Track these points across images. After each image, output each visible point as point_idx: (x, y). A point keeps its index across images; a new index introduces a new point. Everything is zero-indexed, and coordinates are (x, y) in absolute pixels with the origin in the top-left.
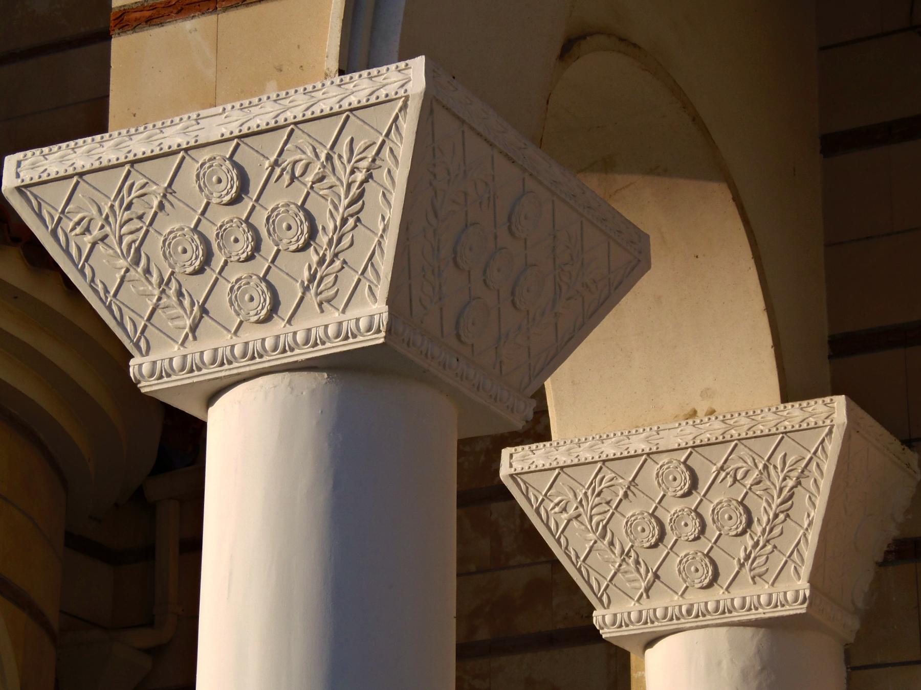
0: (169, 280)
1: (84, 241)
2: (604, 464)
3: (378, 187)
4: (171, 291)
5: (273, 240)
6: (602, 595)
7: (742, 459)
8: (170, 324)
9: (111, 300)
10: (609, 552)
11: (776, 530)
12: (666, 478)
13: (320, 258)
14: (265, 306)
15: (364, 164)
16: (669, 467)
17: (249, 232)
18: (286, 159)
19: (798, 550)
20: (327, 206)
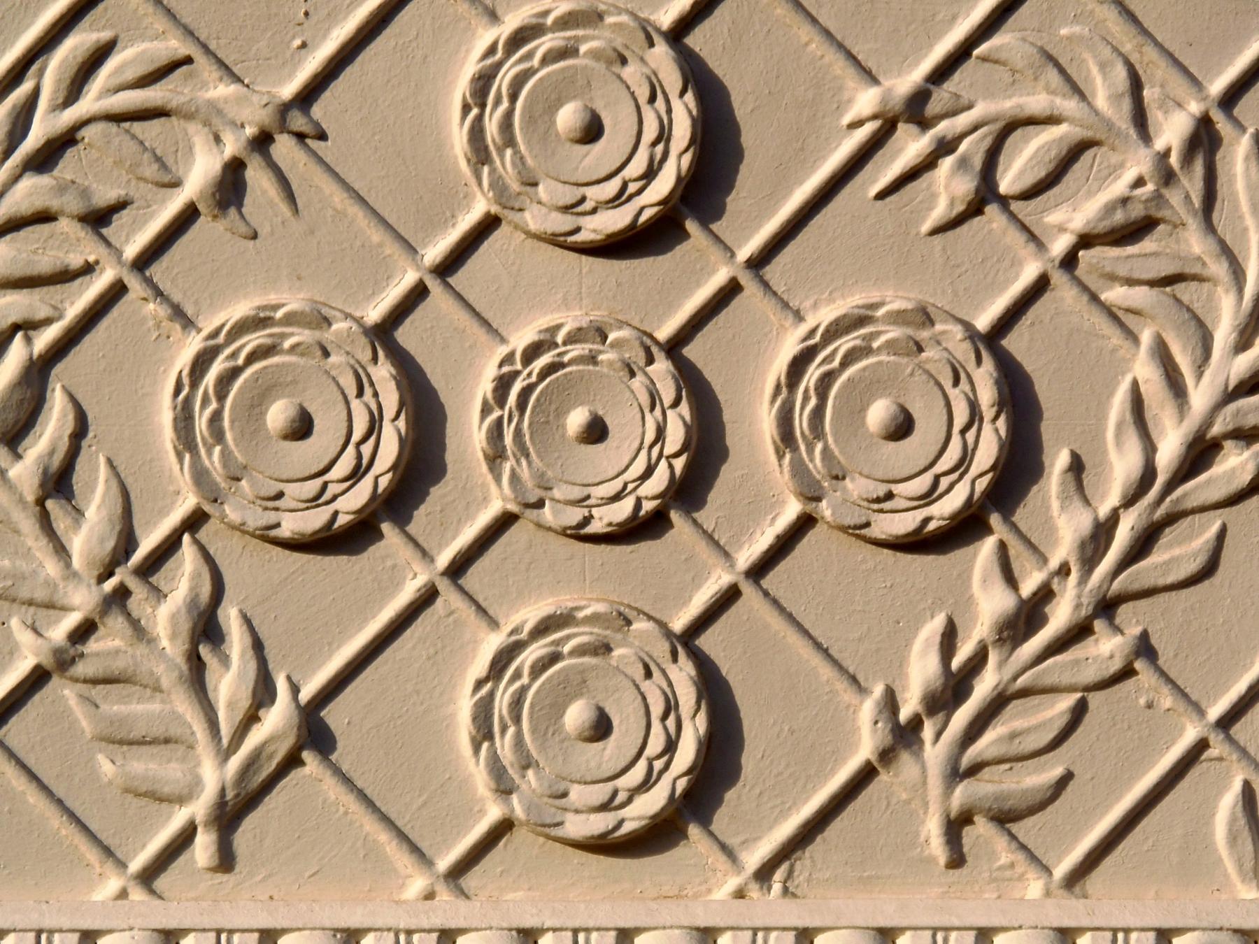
0: (170, 547)
7: (1062, 71)
8: (106, 767)
10: (27, 524)
12: (529, 119)
13: (1022, 603)
14: (661, 772)
17: (676, 403)
18: (966, 96)
20: (1123, 366)
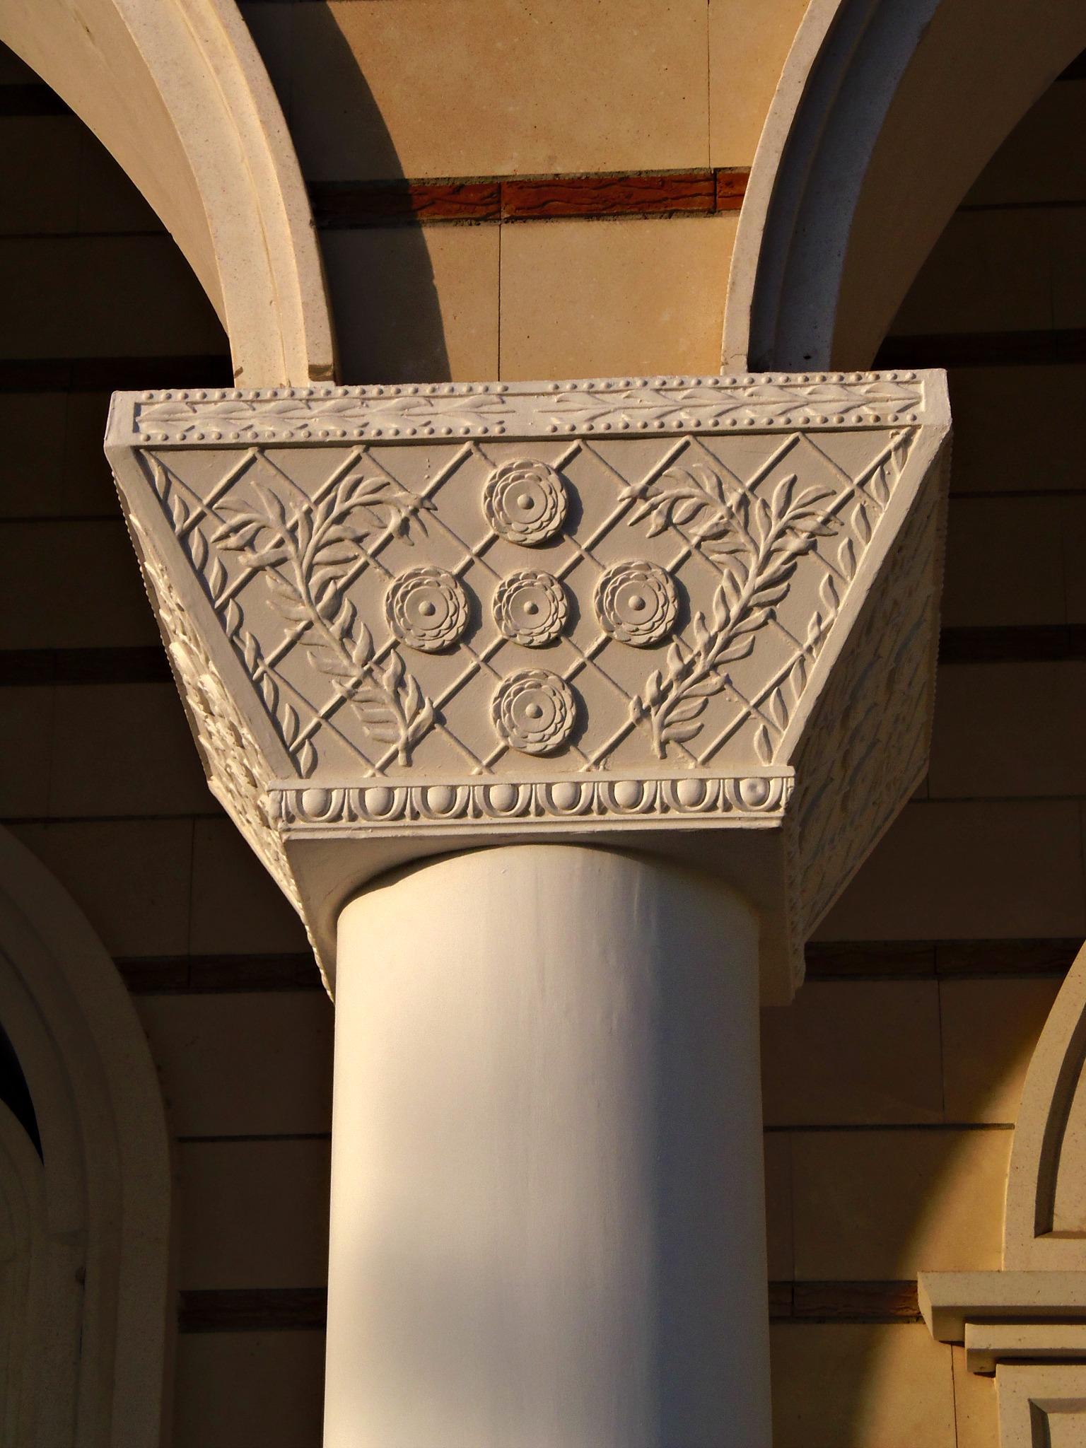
1: (237, 561)
2: (366, 450)
3: (823, 566)
4: (385, 676)
5: (606, 622)
6: (302, 745)
9: (264, 672)
11: (738, 643)
13: (685, 666)
15: (810, 524)
16: (521, 477)
17: (562, 599)
19: (779, 693)
